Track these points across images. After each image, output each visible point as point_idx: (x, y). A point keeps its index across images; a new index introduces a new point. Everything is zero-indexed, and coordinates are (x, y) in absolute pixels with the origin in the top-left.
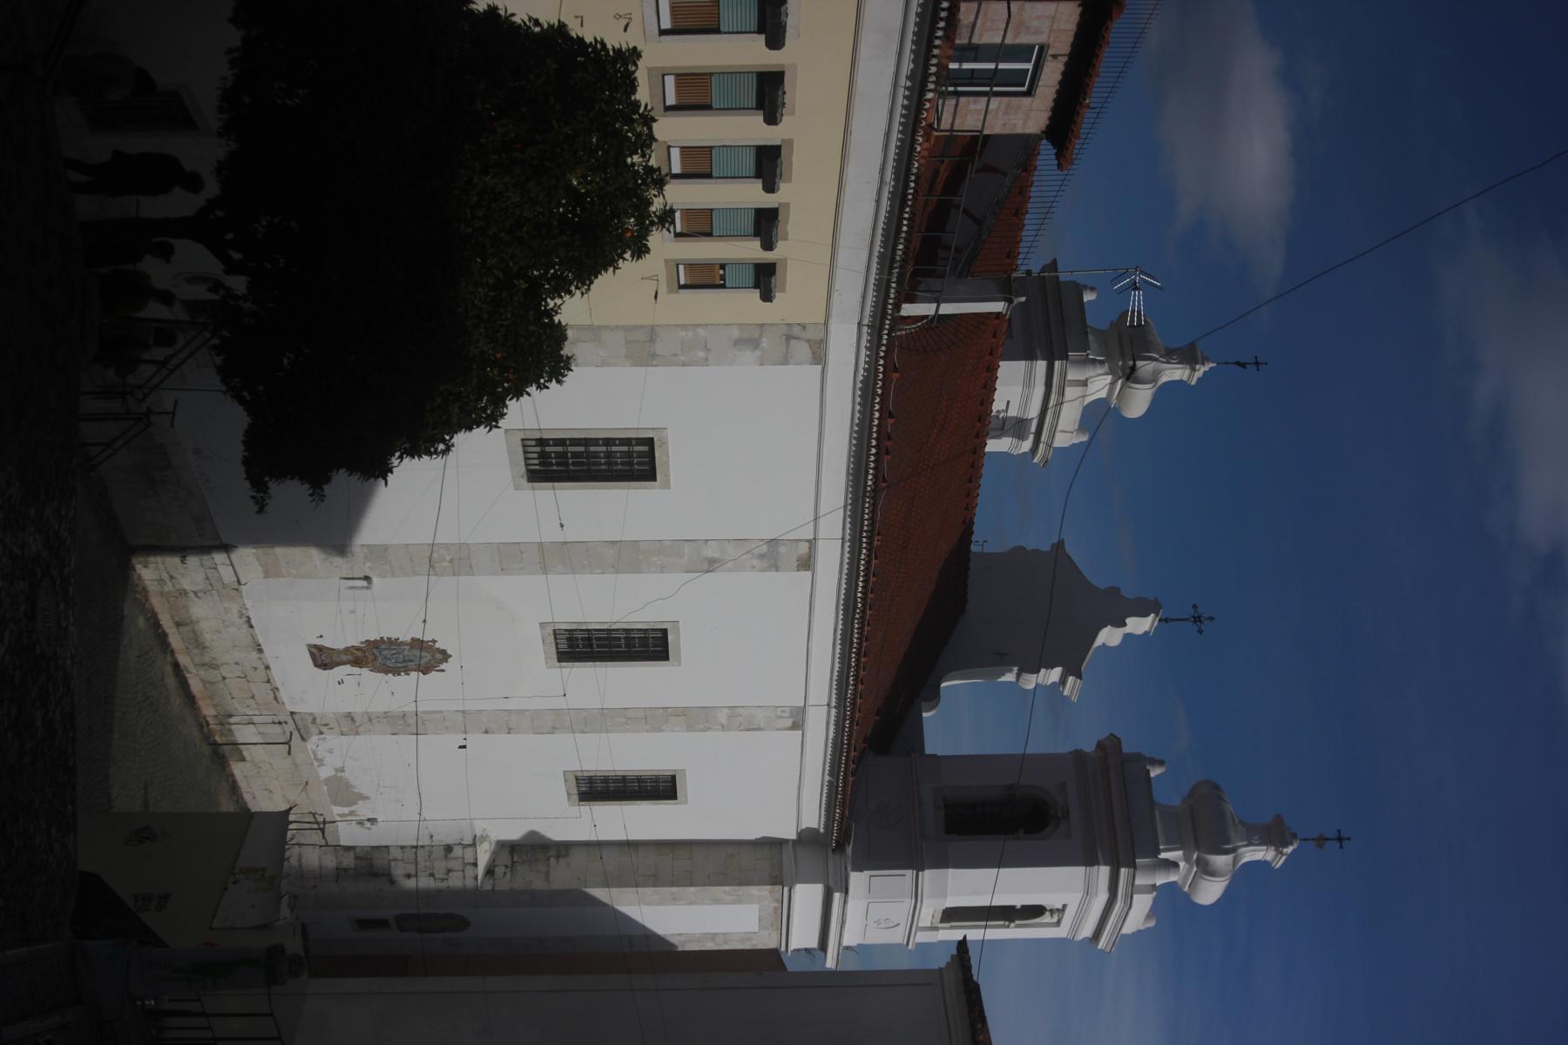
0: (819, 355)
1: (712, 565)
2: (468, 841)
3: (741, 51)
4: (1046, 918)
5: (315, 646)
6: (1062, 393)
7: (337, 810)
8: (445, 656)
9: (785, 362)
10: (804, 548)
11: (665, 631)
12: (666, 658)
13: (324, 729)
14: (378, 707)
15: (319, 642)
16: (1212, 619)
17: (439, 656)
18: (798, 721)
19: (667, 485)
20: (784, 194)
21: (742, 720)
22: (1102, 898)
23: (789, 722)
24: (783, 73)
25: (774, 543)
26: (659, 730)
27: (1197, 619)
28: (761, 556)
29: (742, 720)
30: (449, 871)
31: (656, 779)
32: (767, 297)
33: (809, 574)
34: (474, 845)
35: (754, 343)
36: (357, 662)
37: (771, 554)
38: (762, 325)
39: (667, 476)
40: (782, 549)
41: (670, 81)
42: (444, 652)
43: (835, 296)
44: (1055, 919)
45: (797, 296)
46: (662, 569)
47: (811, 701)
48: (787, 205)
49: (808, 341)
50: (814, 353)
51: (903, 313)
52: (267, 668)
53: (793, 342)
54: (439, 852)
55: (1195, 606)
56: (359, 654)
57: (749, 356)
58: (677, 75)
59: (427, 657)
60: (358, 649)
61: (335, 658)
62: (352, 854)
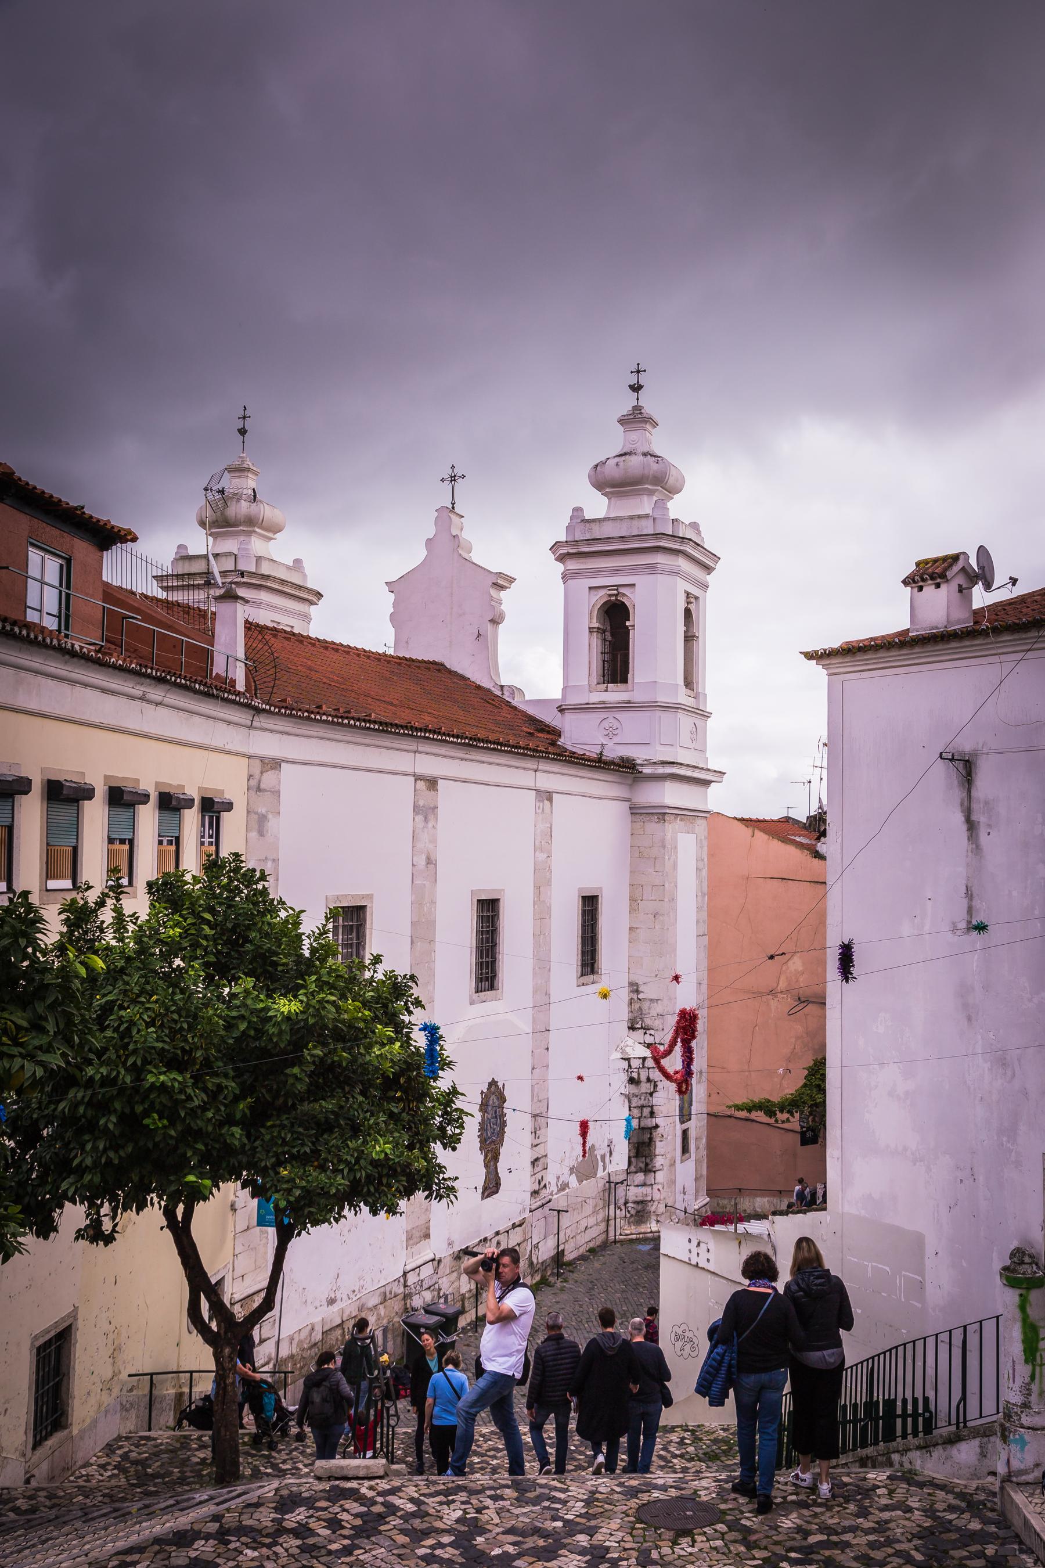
0: (274, 764)
1: (430, 861)
2: (625, 1064)
3: (30, 816)
4: (692, 607)
5: (483, 1193)
6: (267, 577)
7: (600, 1173)
8: (493, 1083)
9: (277, 793)
10: (421, 785)
11: (479, 901)
12: (597, 897)
13: (542, 1184)
14: (528, 1139)
15: (480, 1191)
16: (453, 467)
17: (493, 1087)
18: (546, 796)
19: (370, 897)
20: (148, 785)
21: (544, 841)
22: (682, 563)
23: (547, 803)
24: (49, 782)
25: (416, 809)
26: (549, 908)
27: (453, 479)
28: (426, 820)
29: (544, 841)
30: (649, 1080)
31: (481, 919)
32: (229, 806)
33: (440, 782)
34: (628, 1060)
35: (262, 819)
36: (496, 1158)
37: (425, 812)
38: (248, 812)
39: (363, 897)
40: (421, 803)
41: (52, 884)
42: (490, 1084)
43: (229, 747)
44: (693, 600)
45: (227, 779)
46: (433, 902)
47: (531, 784)
48: (157, 784)
49: (262, 773)
50: (272, 769)
51: (242, 689)
52: (497, 1233)
53: (262, 786)
54: (633, 1090)
55: (442, 480)
56: (489, 1156)
57: (272, 823)
58: (47, 878)
59: (493, 1100)
60: (486, 1156)
61: (492, 1176)
62: (633, 1160)
